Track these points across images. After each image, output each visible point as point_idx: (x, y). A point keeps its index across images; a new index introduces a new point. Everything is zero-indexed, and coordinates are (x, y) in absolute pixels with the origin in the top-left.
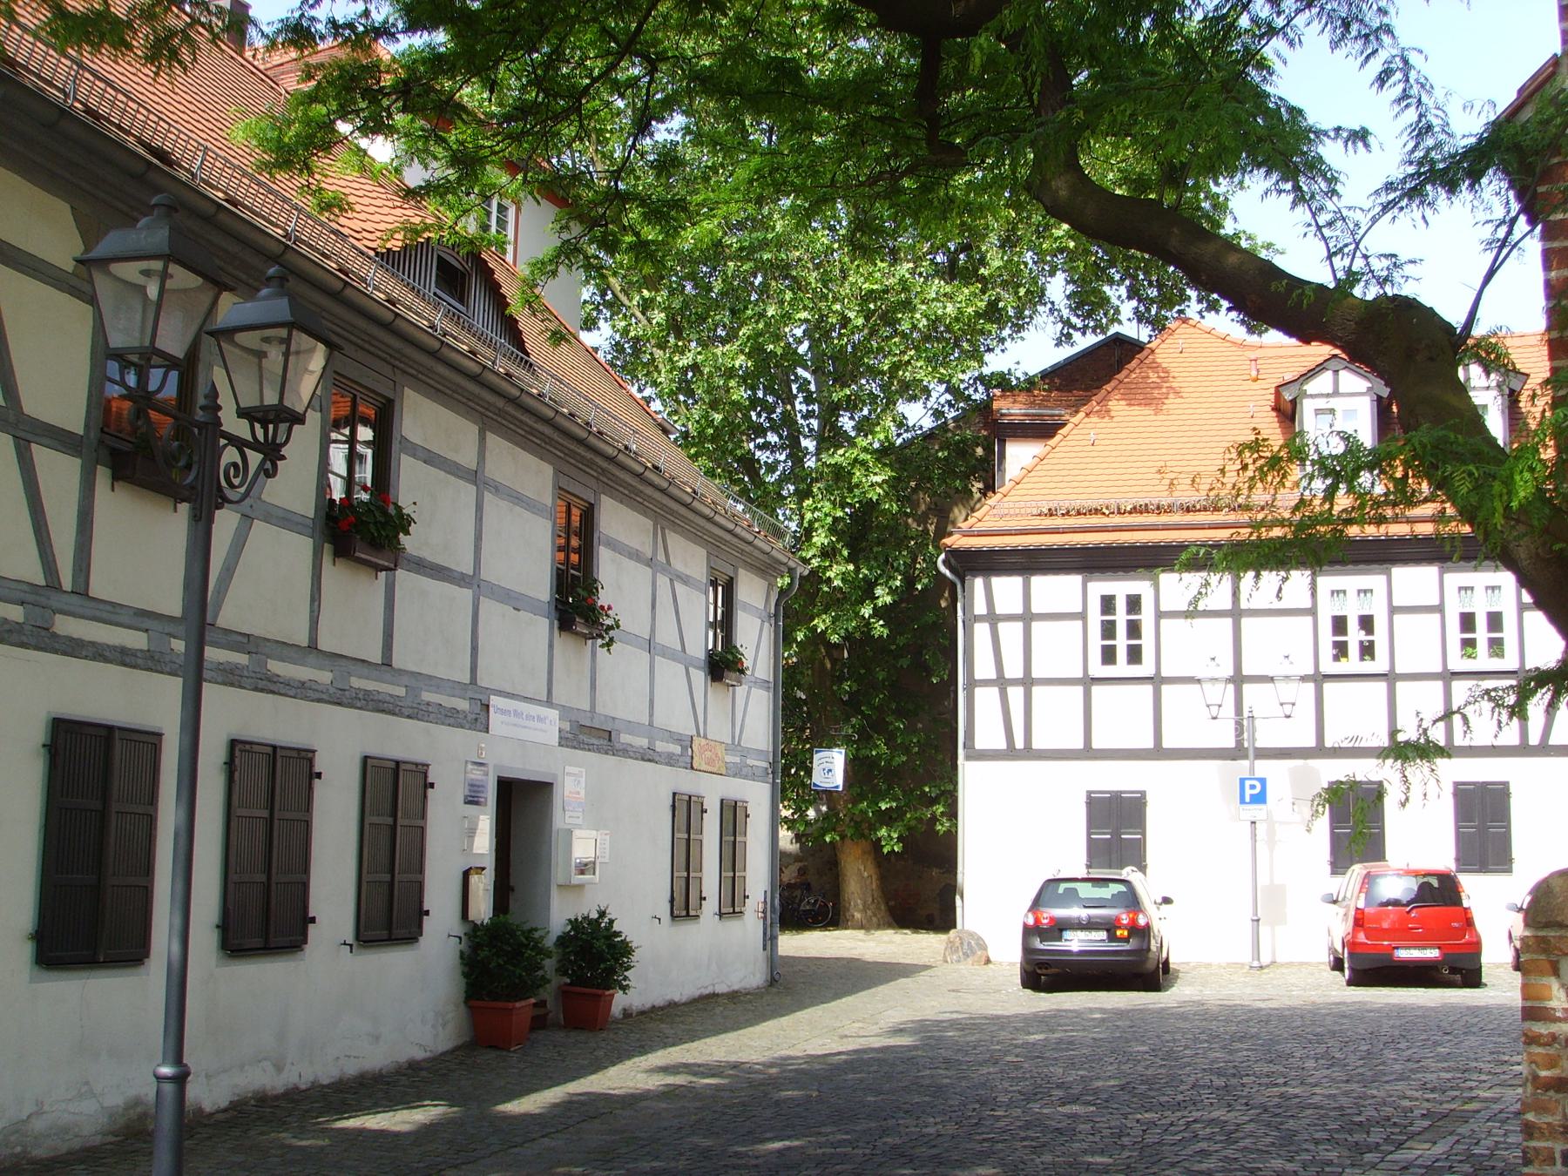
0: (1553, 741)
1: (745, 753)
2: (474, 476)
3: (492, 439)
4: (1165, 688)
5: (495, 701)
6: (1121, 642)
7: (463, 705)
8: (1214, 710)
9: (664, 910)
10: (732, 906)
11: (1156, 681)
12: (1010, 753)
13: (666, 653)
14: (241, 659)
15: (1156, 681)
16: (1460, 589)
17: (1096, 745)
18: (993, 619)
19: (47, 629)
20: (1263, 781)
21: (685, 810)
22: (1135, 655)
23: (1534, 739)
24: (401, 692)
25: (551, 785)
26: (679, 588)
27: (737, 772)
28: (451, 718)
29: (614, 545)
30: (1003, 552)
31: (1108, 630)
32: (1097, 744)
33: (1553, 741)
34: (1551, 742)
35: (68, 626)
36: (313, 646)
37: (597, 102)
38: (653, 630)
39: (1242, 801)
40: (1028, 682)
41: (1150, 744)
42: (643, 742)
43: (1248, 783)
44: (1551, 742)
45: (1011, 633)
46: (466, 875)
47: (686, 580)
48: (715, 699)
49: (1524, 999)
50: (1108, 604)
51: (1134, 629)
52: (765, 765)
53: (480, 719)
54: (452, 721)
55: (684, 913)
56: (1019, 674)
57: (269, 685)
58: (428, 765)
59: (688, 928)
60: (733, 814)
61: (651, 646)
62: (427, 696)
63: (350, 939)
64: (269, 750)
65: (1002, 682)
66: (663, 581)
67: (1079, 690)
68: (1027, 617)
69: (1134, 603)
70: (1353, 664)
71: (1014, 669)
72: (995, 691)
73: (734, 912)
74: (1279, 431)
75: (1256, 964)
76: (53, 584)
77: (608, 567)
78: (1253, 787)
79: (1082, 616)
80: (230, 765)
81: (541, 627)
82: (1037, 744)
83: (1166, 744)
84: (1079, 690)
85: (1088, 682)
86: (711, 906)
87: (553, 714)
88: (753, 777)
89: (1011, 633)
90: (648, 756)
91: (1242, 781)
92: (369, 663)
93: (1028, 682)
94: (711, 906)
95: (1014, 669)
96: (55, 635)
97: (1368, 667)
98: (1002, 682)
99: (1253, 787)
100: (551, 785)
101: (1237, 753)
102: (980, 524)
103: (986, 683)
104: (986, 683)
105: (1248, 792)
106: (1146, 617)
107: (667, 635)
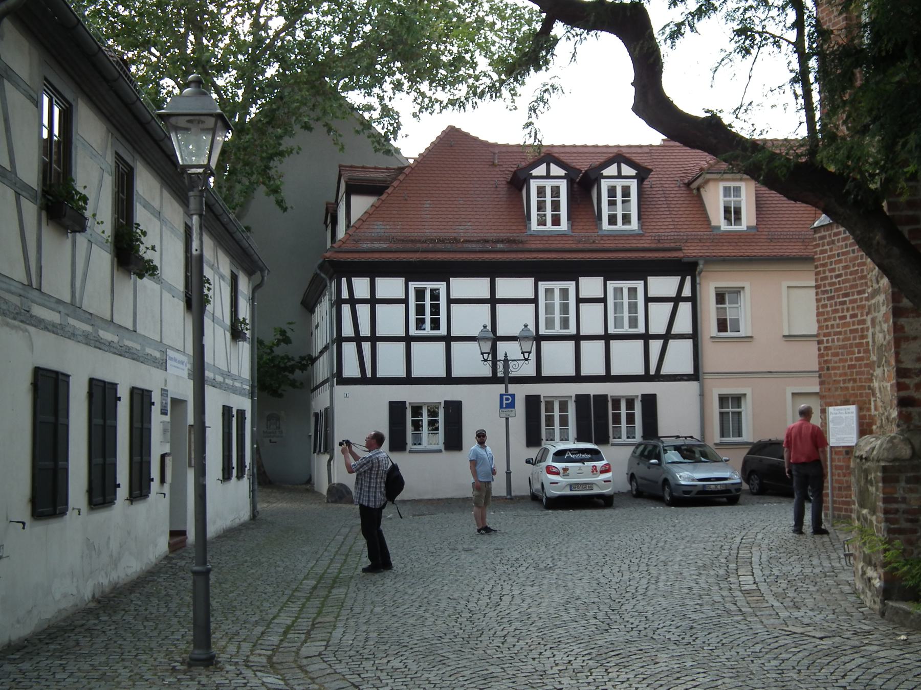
0: (664, 371)
4: (454, 345)
5: (170, 353)
6: (428, 317)
7: (157, 354)
11: (448, 339)
12: (363, 380)
15: (448, 339)
16: (788, 287)
17: (415, 374)
18: (353, 302)
19: (28, 312)
20: (513, 396)
22: (435, 324)
23: (652, 372)
24: (139, 348)
30: (359, 263)
31: (420, 310)
33: (664, 371)
34: (662, 373)
36: (112, 321)
38: (214, 311)
39: (501, 407)
40: (374, 339)
41: (443, 374)
43: (505, 397)
44: (662, 373)
45: (363, 311)
50: (420, 294)
51: (435, 309)
52: (248, 388)
54: (155, 365)
56: (367, 296)
57: (100, 344)
58: (151, 391)
63: (221, 479)
64: (102, 384)
65: (358, 339)
67: (602, 343)
68: (373, 301)
69: (435, 296)
70: (428, 331)
71: (365, 331)
72: (353, 345)
74: (505, 189)
75: (509, 497)
78: (507, 399)
79: (405, 301)
80: (91, 395)
82: (380, 374)
83: (614, 372)
84: (602, 343)
85: (408, 340)
89: (363, 311)
91: (501, 396)
92: (127, 329)
93: (374, 339)
95: (365, 331)
96: (32, 316)
97: (633, 331)
98: (358, 339)
99: (507, 399)
101: (493, 380)
102: (344, 245)
103: (349, 339)
105: (505, 402)
106: (443, 302)
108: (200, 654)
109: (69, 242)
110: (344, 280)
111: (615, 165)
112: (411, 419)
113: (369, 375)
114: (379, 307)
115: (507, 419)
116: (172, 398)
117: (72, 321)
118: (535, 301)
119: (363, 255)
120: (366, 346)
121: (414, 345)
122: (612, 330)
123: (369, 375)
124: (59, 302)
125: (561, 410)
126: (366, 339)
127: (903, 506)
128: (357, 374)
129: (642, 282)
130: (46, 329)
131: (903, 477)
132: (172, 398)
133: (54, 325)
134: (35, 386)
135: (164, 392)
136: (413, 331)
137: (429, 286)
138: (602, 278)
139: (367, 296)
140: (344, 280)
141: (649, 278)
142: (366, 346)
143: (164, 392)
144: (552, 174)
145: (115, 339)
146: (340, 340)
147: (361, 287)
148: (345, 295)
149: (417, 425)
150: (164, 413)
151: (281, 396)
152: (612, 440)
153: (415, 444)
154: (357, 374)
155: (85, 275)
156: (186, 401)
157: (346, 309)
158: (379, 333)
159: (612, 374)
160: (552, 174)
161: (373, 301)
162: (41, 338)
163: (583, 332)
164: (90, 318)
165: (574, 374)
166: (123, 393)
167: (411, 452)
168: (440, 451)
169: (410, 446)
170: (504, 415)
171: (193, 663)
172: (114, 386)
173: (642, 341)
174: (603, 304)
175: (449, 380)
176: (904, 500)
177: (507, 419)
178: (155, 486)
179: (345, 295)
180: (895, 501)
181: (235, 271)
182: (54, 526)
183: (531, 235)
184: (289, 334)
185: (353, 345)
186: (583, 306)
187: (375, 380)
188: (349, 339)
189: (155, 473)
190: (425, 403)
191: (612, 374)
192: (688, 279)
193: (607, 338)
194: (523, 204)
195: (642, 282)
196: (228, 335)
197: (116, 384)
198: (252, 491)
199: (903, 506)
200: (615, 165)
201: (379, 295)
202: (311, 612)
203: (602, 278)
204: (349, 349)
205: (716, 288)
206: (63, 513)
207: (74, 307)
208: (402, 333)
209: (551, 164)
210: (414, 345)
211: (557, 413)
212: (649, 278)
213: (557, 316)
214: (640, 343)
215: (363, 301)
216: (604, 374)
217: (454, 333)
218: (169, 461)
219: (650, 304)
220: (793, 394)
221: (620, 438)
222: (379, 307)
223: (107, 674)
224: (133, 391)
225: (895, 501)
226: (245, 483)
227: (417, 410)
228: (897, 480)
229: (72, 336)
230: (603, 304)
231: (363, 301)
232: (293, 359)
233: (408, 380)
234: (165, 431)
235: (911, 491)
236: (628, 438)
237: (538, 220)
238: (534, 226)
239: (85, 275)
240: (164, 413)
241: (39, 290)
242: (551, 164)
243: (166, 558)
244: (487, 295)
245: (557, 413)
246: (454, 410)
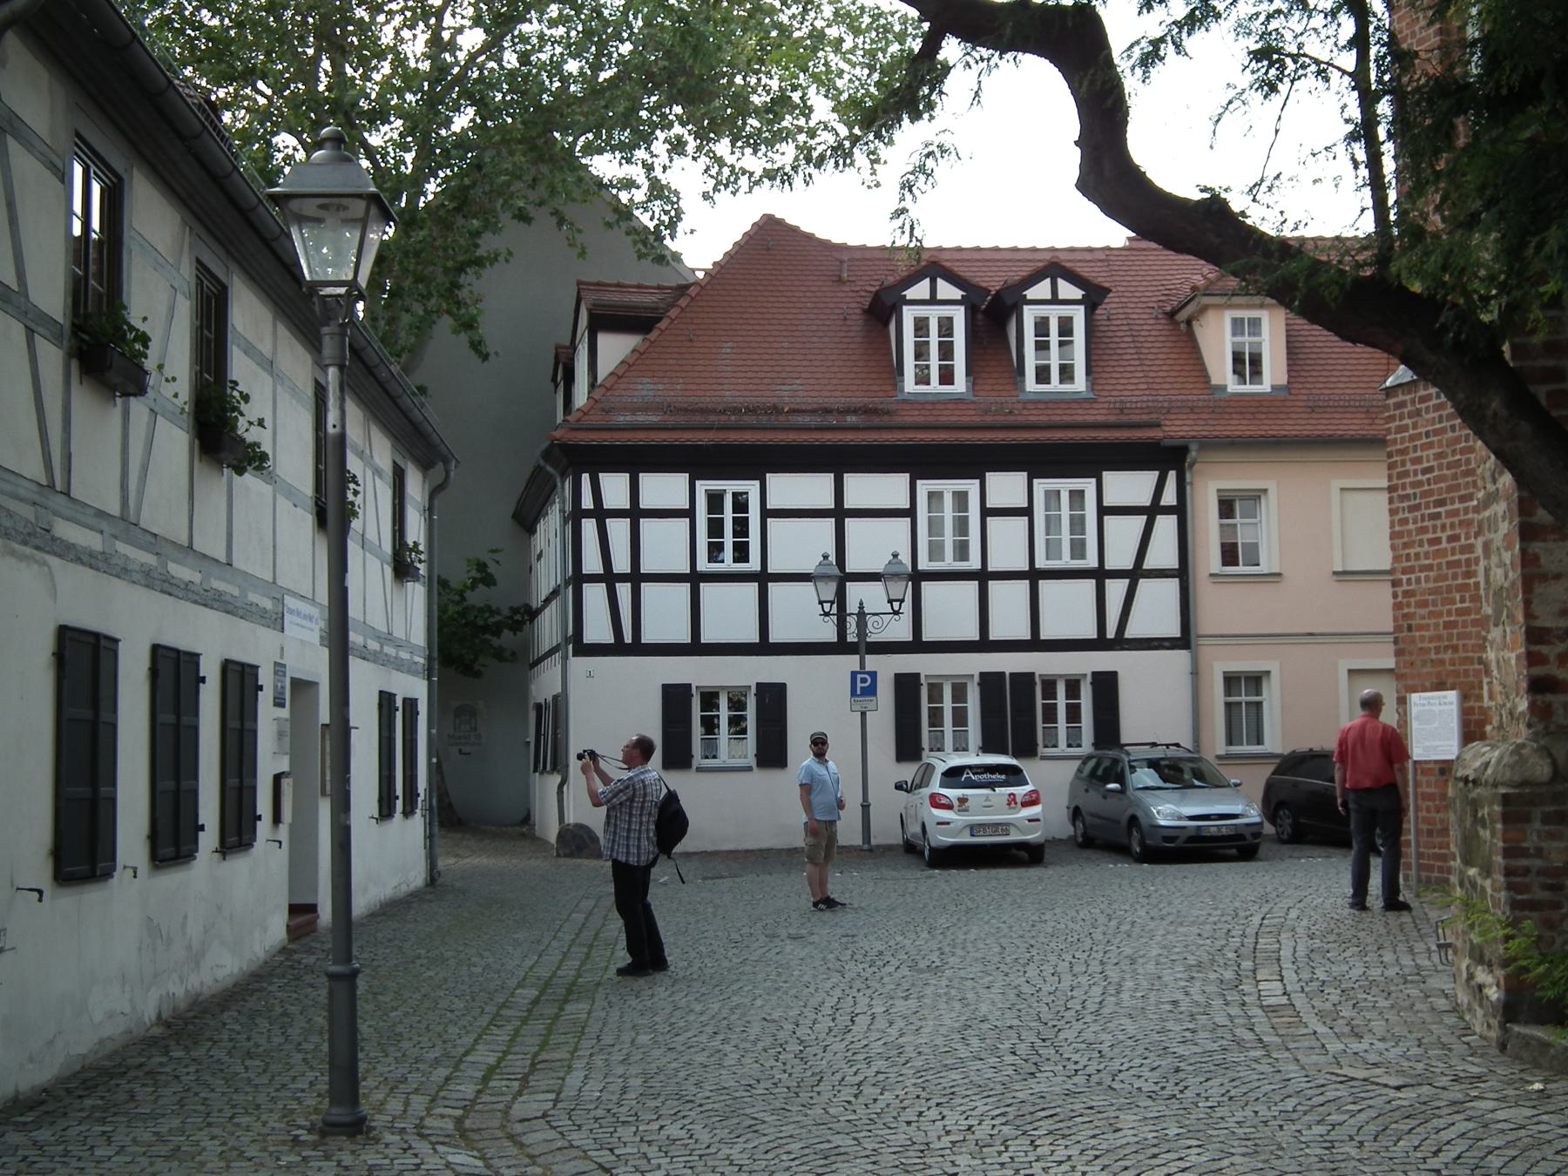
0: (1130, 633)
4: (773, 588)
5: (290, 602)
7: (267, 604)
8: (896, 605)
9: (39, 870)
11: (763, 578)
12: (618, 648)
15: (763, 578)
17: (707, 637)
18: (601, 514)
19: (48, 531)
20: (873, 675)
22: (741, 553)
23: (1111, 634)
24: (236, 592)
30: (611, 448)
31: (715, 528)
33: (1130, 633)
34: (1127, 635)
36: (190, 547)
37: (636, 172)
38: (364, 530)
39: (853, 693)
40: (637, 578)
41: (754, 638)
43: (859, 676)
44: (1127, 635)
45: (619, 530)
50: (715, 501)
51: (741, 527)
52: (422, 661)
54: (264, 621)
56: (625, 504)
57: (169, 587)
58: (257, 667)
63: (376, 816)
64: (174, 655)
65: (609, 578)
67: (1024, 585)
68: (635, 513)
69: (740, 504)
70: (728, 564)
71: (622, 564)
72: (601, 588)
75: (866, 847)
78: (863, 680)
79: (690, 514)
82: (647, 637)
83: (1045, 634)
84: (1024, 585)
85: (695, 579)
86: (209, 839)
89: (619, 530)
91: (854, 674)
92: (217, 561)
93: (637, 578)
94: (209, 839)
95: (622, 564)
96: (54, 539)
97: (1078, 564)
98: (609, 578)
99: (863, 680)
101: (840, 647)
102: (586, 418)
103: (594, 578)
105: (859, 685)
106: (754, 515)
108: (340, 1114)
109: (117, 412)
110: (586, 477)
111: (1048, 281)
112: (700, 713)
113: (628, 639)
114: (645, 524)
115: (863, 714)
116: (293, 679)
117: (122, 548)
118: (910, 513)
119: (617, 435)
120: (624, 590)
121: (705, 588)
122: (1041, 563)
123: (628, 639)
124: (101, 514)
125: (955, 699)
126: (623, 578)
127: (1537, 863)
128: (608, 637)
129: (1093, 481)
130: (78, 560)
131: (1537, 813)
132: (293, 679)
133: (91, 554)
134: (60, 658)
135: (279, 668)
136: (703, 565)
137: (730, 487)
138: (1025, 474)
139: (625, 504)
140: (586, 477)
141: (1104, 473)
142: (624, 590)
143: (279, 668)
144: (940, 297)
145: (196, 577)
146: (578, 579)
147: (615, 489)
148: (587, 502)
149: (710, 725)
150: (279, 703)
151: (478, 675)
152: (1041, 750)
153: (707, 757)
154: (608, 637)
155: (145, 468)
156: (317, 684)
157: (589, 527)
158: (646, 568)
159: (1042, 637)
160: (940, 297)
161: (635, 513)
162: (70, 576)
163: (992, 566)
164: (153, 542)
165: (977, 638)
166: (210, 669)
167: (699, 770)
168: (749, 769)
169: (698, 760)
170: (857, 707)
171: (328, 1129)
172: (194, 658)
173: (1094, 581)
174: (1026, 519)
175: (764, 647)
176: (1539, 852)
177: (863, 714)
178: (264, 828)
179: (587, 502)
180: (1524, 853)
181: (400, 462)
182: (92, 896)
183: (904, 401)
185: (601, 588)
186: (992, 522)
187: (639, 648)
188: (594, 578)
189: (264, 805)
190: (723, 688)
191: (1042, 637)
192: (1172, 475)
193: (1034, 576)
194: (890, 348)
195: (1093, 481)
196: (389, 571)
197: (198, 655)
198: (430, 837)
199: (1537, 863)
200: (1048, 281)
201: (646, 502)
203: (1025, 474)
204: (594, 595)
205: (1218, 490)
206: (108, 874)
207: (126, 524)
208: (685, 568)
209: (939, 280)
210: (705, 588)
211: (948, 705)
212: (1104, 473)
213: (949, 538)
214: (1090, 584)
215: (618, 514)
216: (1028, 637)
217: (773, 568)
218: (287, 785)
219: (1106, 518)
220: (1350, 671)
221: (1055, 746)
222: (645, 524)
223: (183, 1149)
224: (227, 666)
225: (1524, 853)
226: (417, 823)
227: (710, 699)
228: (1527, 819)
229: (123, 572)
230: (1026, 519)
231: (618, 514)
232: (498, 612)
233: (695, 647)
234: (281, 734)
235: (1552, 836)
236: (1069, 746)
237: (916, 375)
238: (910, 385)
239: (145, 468)
240: (279, 703)
241: (67, 494)
242: (939, 280)
243: (283, 950)
244: (829, 503)
245: (948, 705)
246: (773, 698)
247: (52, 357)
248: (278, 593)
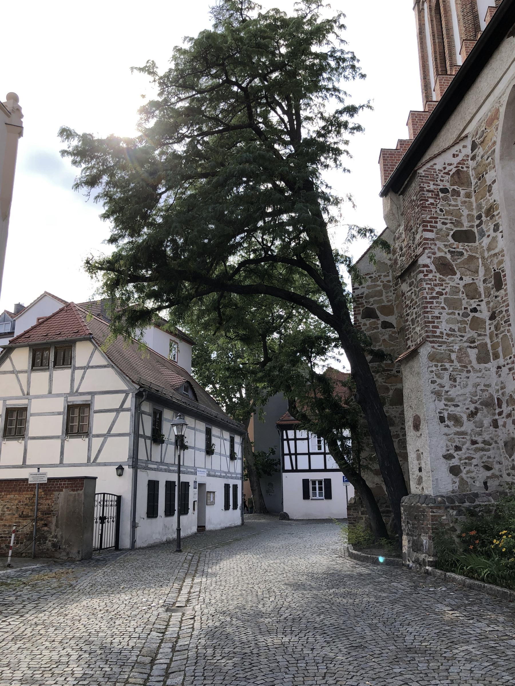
1: (237, 474)
2: (194, 429)
3: (197, 421)
7: (193, 471)
10: (235, 507)
12: (292, 471)
13: (223, 455)
14: (166, 467)
17: (312, 468)
18: (288, 440)
21: (227, 486)
25: (205, 484)
26: (225, 441)
27: (236, 478)
28: (192, 473)
29: (214, 436)
32: (312, 468)
35: (150, 466)
39: (344, 481)
40: (296, 454)
42: (219, 474)
45: (292, 443)
46: (194, 502)
47: (226, 440)
48: (232, 464)
49: (348, 515)
53: (195, 474)
55: (106, 495)
56: (293, 437)
59: (227, 511)
60: (235, 487)
61: (220, 454)
62: (189, 470)
65: (290, 454)
66: (222, 440)
68: (295, 439)
71: (293, 451)
72: (288, 456)
73: (104, 494)
76: (148, 460)
77: (214, 440)
81: (204, 454)
87: (205, 470)
88: (238, 479)
89: (292, 443)
90: (220, 477)
93: (296, 454)
95: (293, 451)
98: (290, 454)
100: (205, 484)
103: (287, 454)
104: (287, 454)
107: (223, 452)
108: (178, 549)
109: (160, 446)
110: (284, 432)
113: (295, 469)
115: (346, 486)
116: (199, 484)
120: (293, 457)
123: (295, 469)
124: (156, 462)
125: (315, 488)
126: (293, 454)
127: (352, 517)
128: (290, 468)
130: (153, 470)
131: (352, 509)
132: (199, 484)
133: (155, 469)
134: (149, 485)
139: (293, 437)
140: (284, 432)
142: (293, 457)
143: (195, 482)
147: (291, 434)
149: (314, 489)
150: (195, 488)
151: (271, 475)
154: (290, 468)
155: (165, 453)
157: (285, 443)
161: (295, 439)
164: (167, 464)
167: (312, 499)
169: (311, 497)
171: (177, 551)
175: (325, 470)
176: (352, 515)
177: (346, 486)
178: (191, 510)
179: (285, 437)
180: (350, 515)
181: (232, 436)
182: (154, 520)
184: (274, 450)
185: (288, 456)
187: (297, 471)
196: (228, 459)
198: (242, 515)
199: (352, 517)
202: (504, 638)
206: (156, 517)
207: (162, 463)
215: (292, 439)
218: (196, 503)
223: (321, 678)
225: (350, 515)
226: (238, 511)
227: (314, 482)
228: (351, 509)
229: (161, 470)
231: (292, 439)
232: (275, 460)
233: (310, 470)
234: (195, 494)
235: (354, 512)
239: (165, 453)
240: (195, 488)
241: (151, 460)
243: (196, 533)
246: (328, 482)
247: (148, 442)
248: (195, 468)
